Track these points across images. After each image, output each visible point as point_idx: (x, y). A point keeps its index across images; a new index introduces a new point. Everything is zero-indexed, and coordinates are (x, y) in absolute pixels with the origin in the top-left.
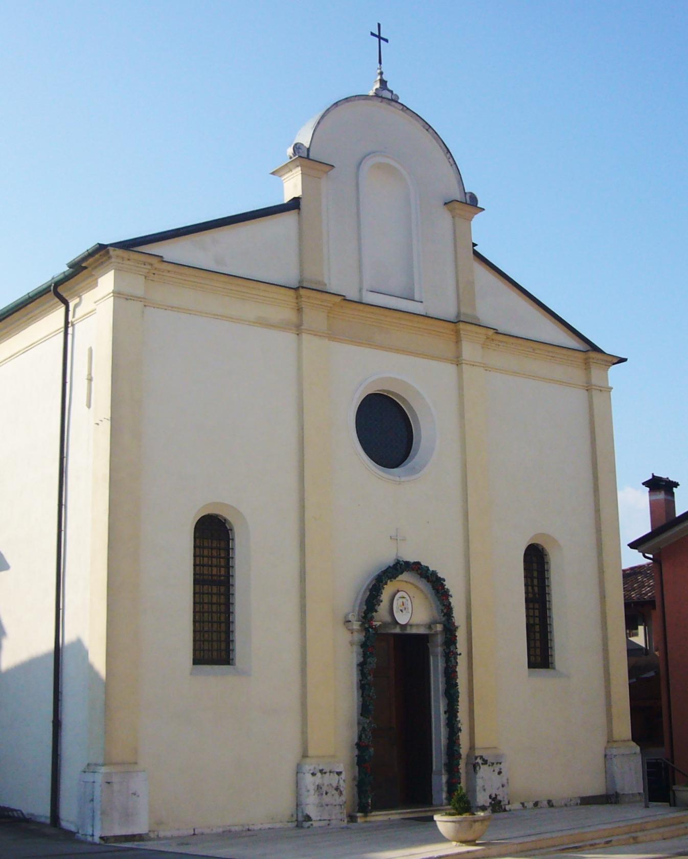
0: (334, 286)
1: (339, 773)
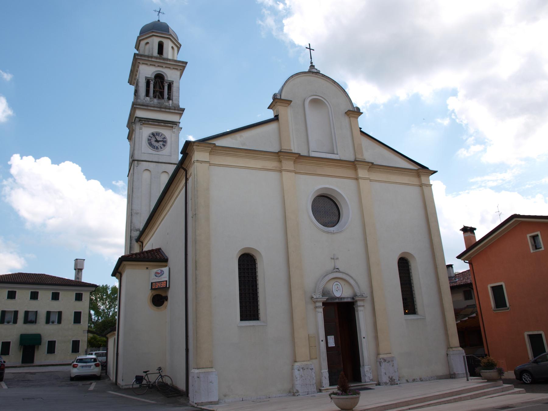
0: (295, 150)
1: (312, 369)
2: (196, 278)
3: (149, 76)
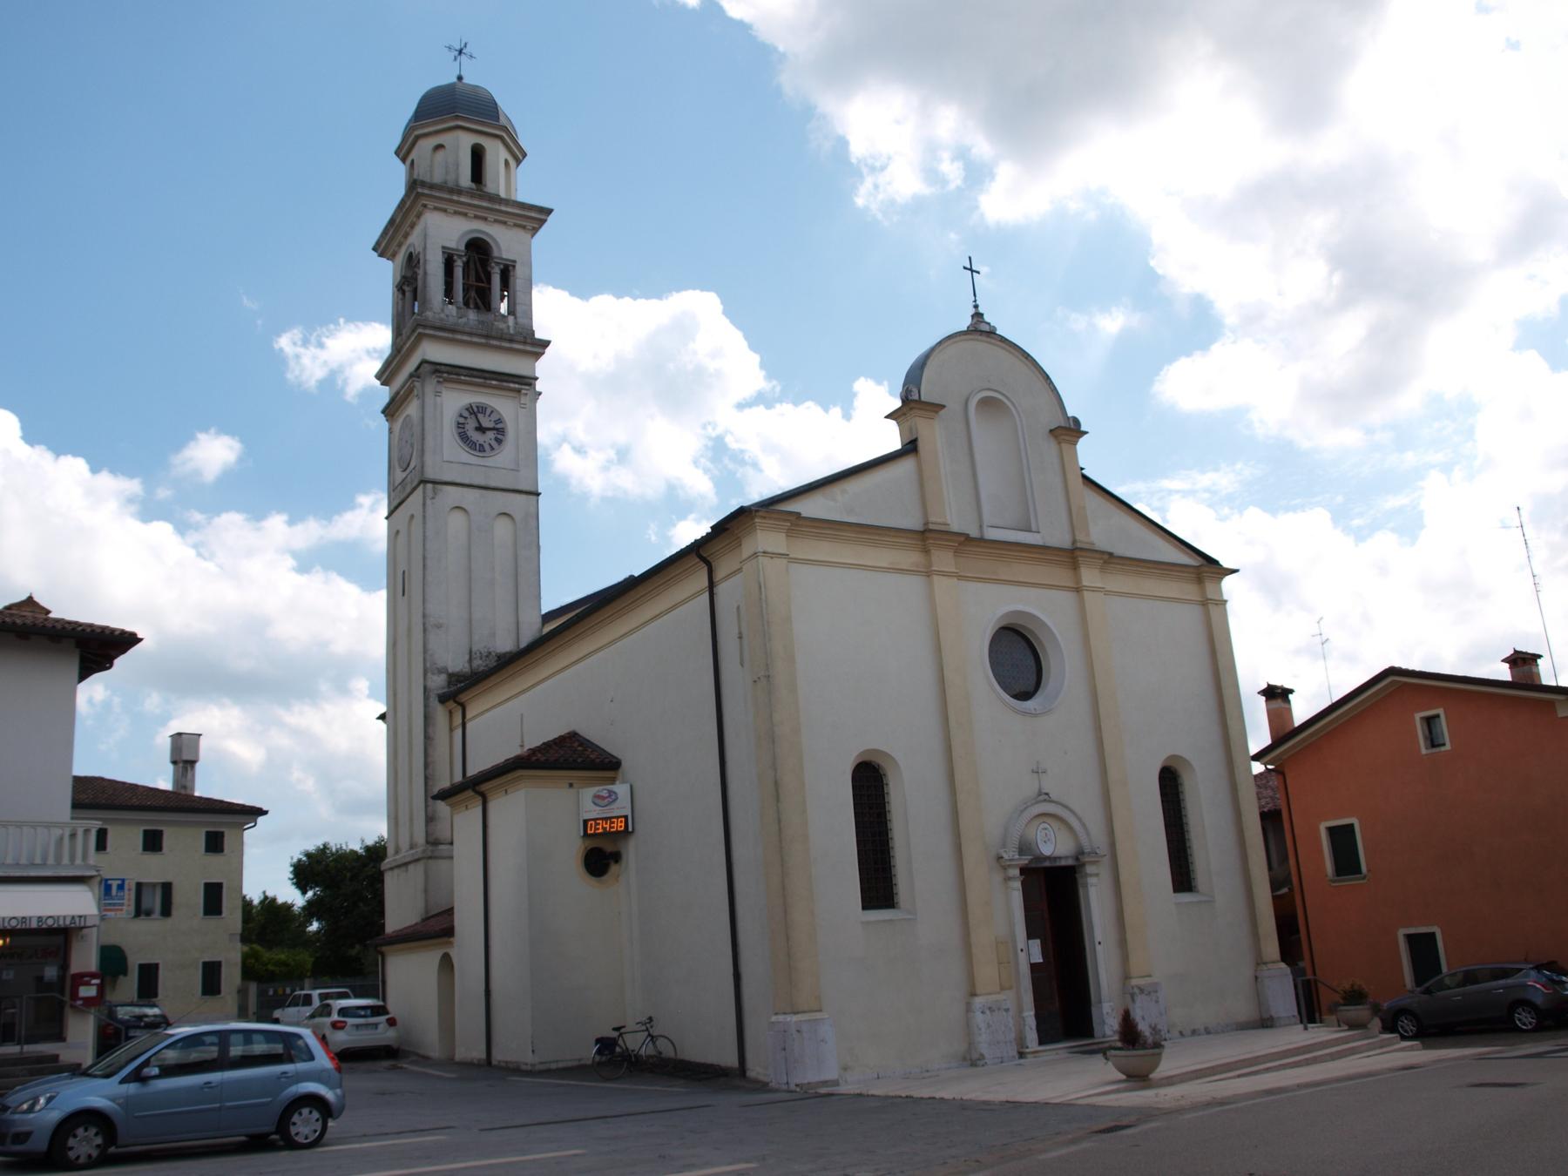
0: (955, 528)
1: (1007, 1010)
2: (779, 821)
3: (452, 245)
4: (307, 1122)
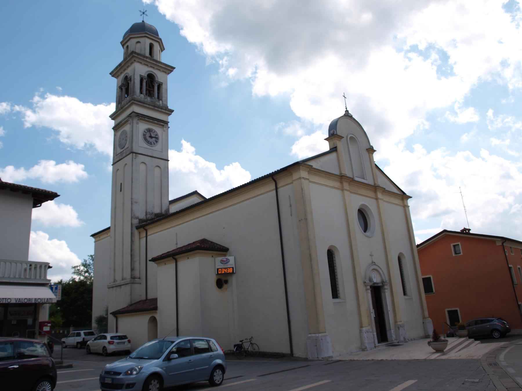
2: (312, 268)
3: (143, 75)
4: (218, 375)
